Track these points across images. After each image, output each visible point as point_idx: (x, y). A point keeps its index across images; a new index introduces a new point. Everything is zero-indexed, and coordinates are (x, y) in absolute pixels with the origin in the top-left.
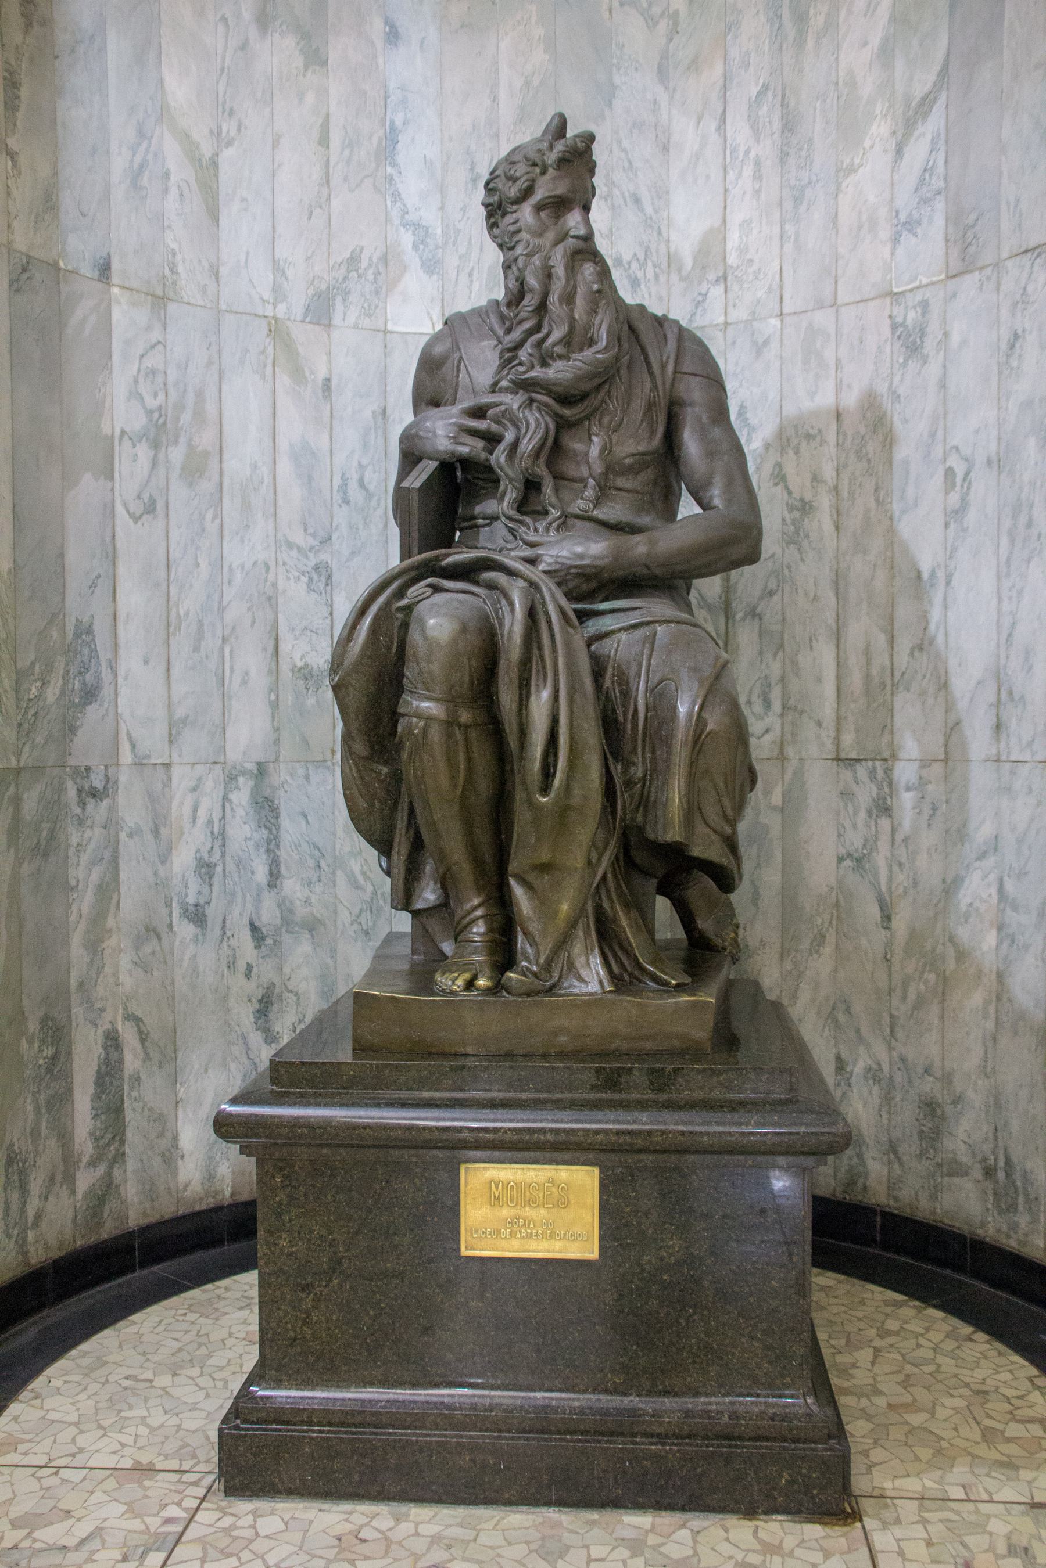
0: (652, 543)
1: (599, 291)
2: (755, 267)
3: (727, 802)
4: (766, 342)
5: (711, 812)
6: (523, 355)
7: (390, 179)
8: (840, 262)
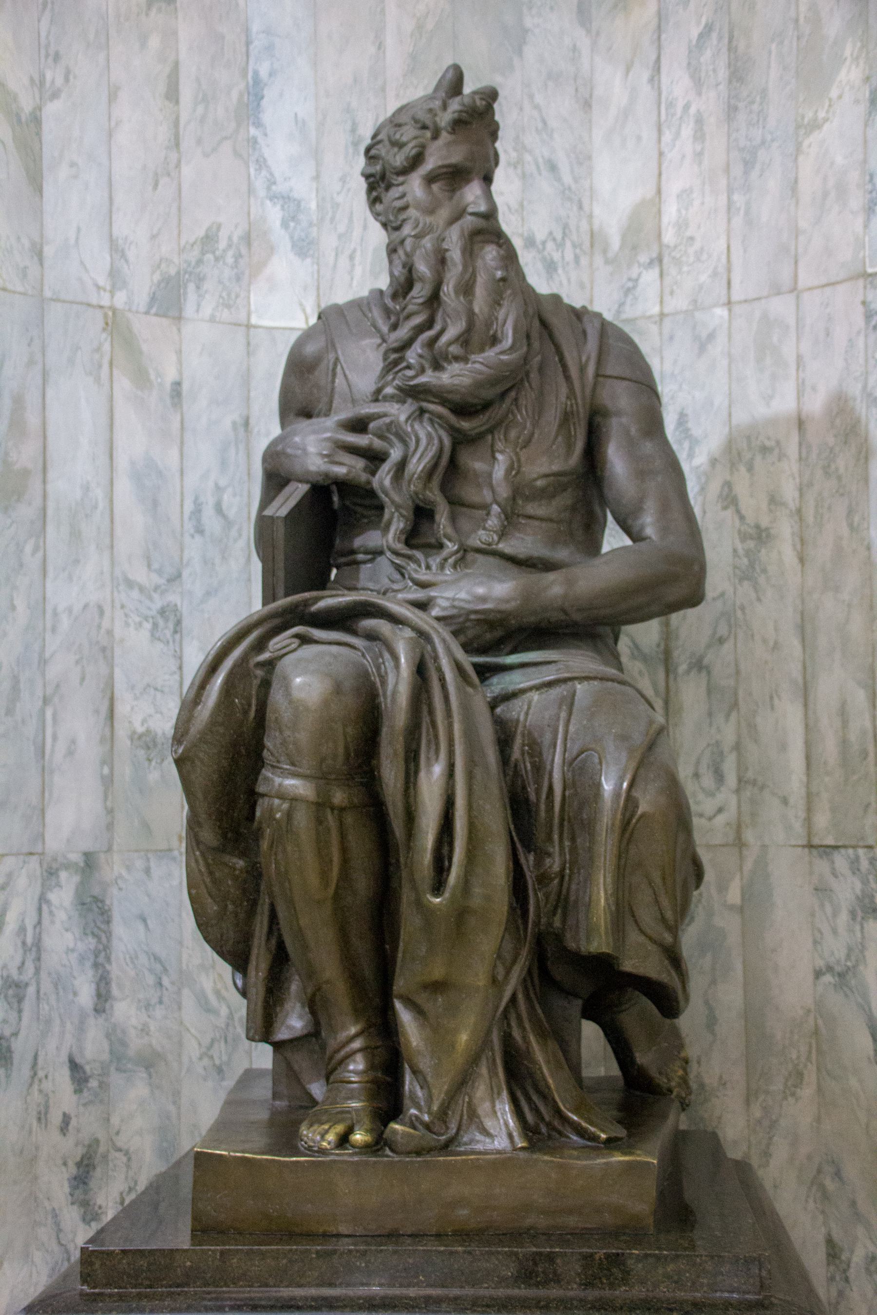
0: (570, 582)
1: (503, 279)
2: (697, 245)
3: (665, 902)
4: (711, 336)
5: (647, 916)
6: (412, 356)
7: (253, 142)
8: (801, 238)
